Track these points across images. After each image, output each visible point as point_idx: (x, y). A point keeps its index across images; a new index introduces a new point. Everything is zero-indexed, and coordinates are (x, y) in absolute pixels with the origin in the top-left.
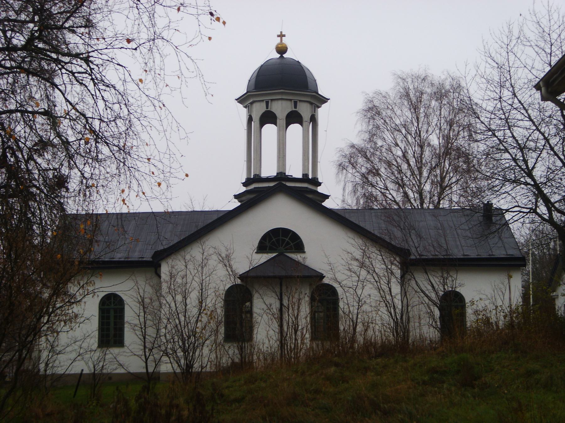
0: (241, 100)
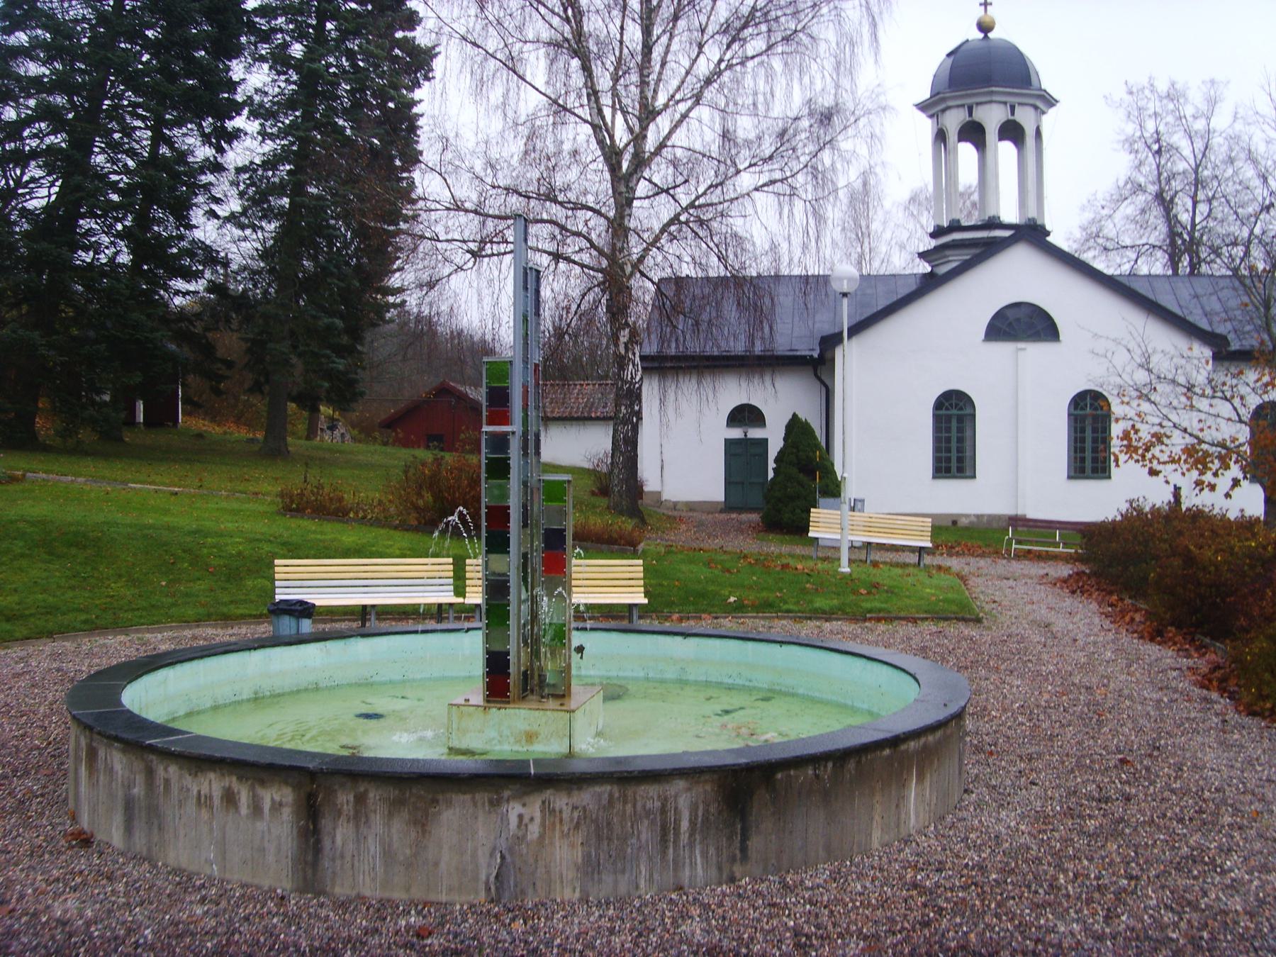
0: (923, 107)
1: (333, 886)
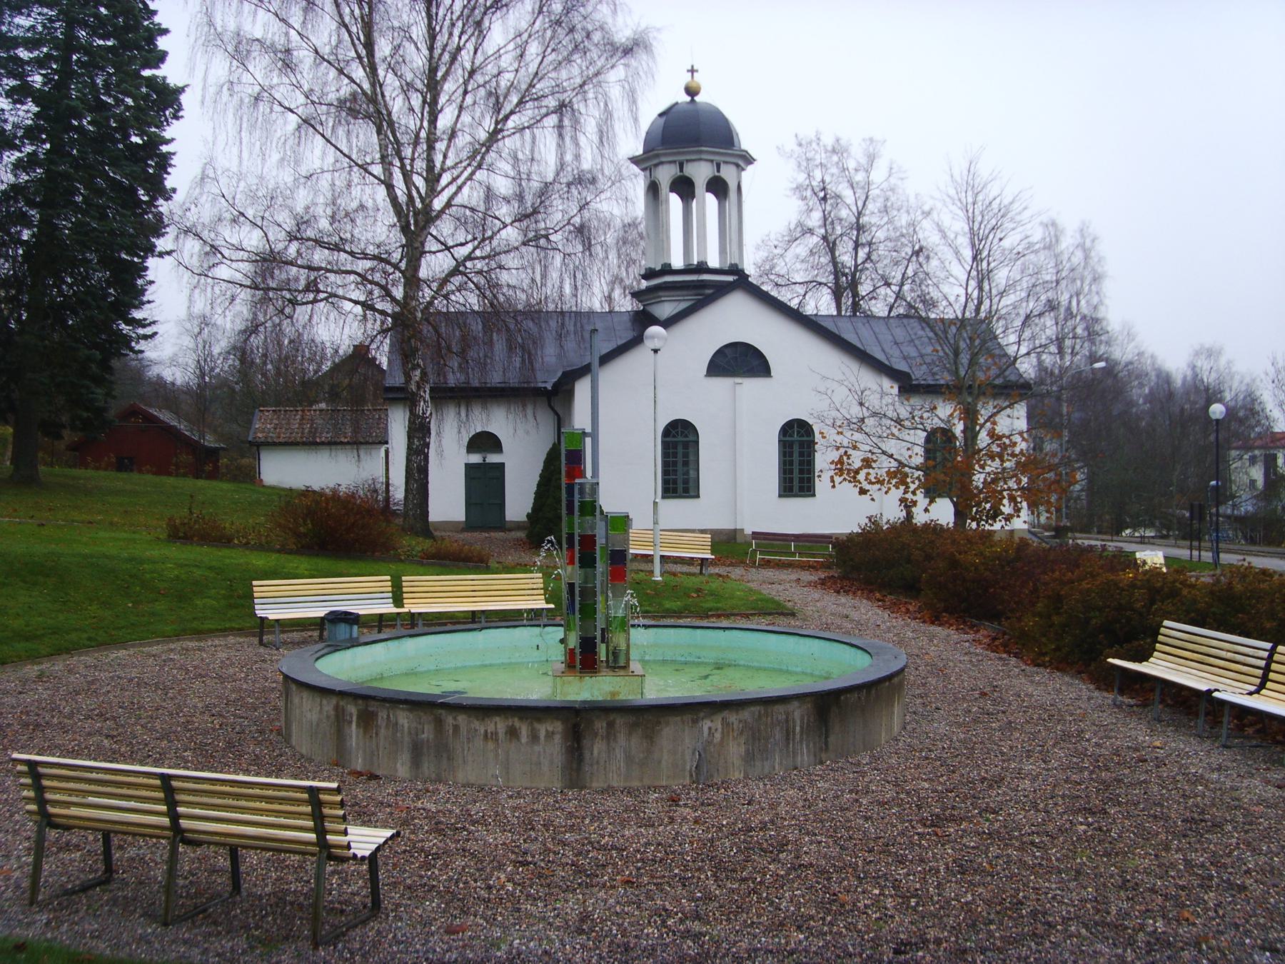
1: (591, 781)
